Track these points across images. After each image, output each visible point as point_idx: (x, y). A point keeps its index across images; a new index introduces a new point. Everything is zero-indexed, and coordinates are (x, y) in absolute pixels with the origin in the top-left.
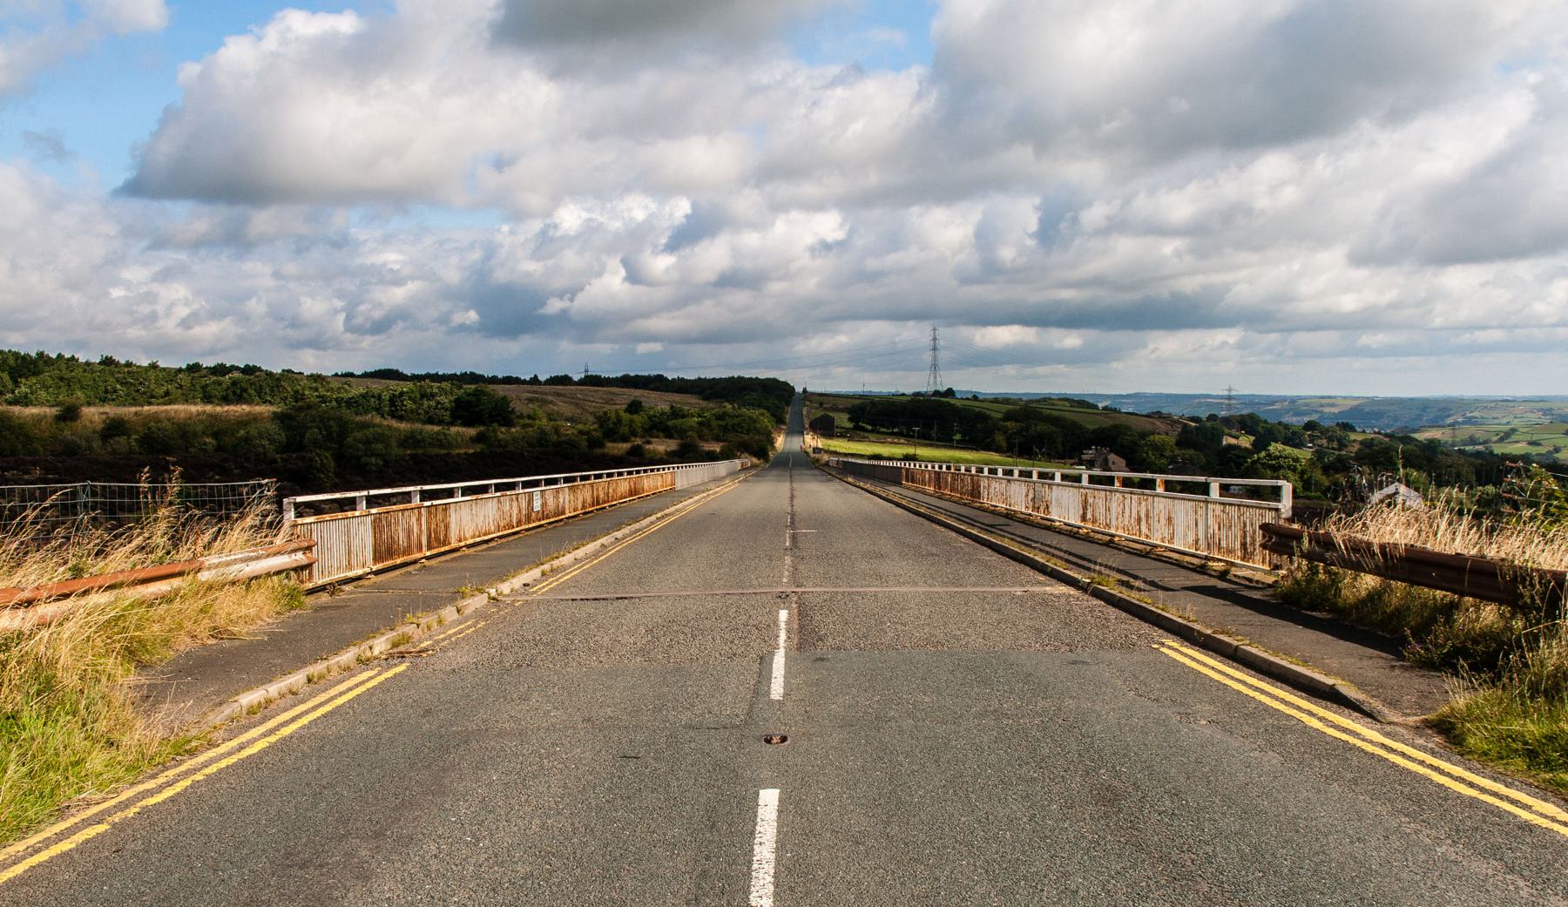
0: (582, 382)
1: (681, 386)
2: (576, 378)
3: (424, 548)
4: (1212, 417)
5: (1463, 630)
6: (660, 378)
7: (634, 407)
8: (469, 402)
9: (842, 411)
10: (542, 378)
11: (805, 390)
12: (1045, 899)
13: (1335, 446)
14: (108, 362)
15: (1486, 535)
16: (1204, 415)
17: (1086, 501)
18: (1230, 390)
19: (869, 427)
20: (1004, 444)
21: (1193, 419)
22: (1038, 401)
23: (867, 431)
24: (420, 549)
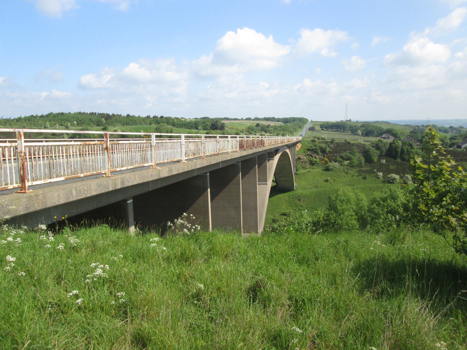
0: (254, 120)
1: (278, 120)
2: (253, 118)
3: (91, 171)
4: (423, 126)
5: (392, 344)
6: (274, 118)
7: (258, 125)
8: (214, 124)
9: (318, 125)
10: (244, 118)
11: (312, 120)
12: (375, 241)
13: (458, 133)
14: (128, 115)
15: (385, 287)
16: (420, 125)
17: (15, 192)
18: (428, 118)
19: (325, 130)
20: (360, 133)
21: (417, 126)
22: (375, 122)
23: (325, 130)
24: (90, 171)
